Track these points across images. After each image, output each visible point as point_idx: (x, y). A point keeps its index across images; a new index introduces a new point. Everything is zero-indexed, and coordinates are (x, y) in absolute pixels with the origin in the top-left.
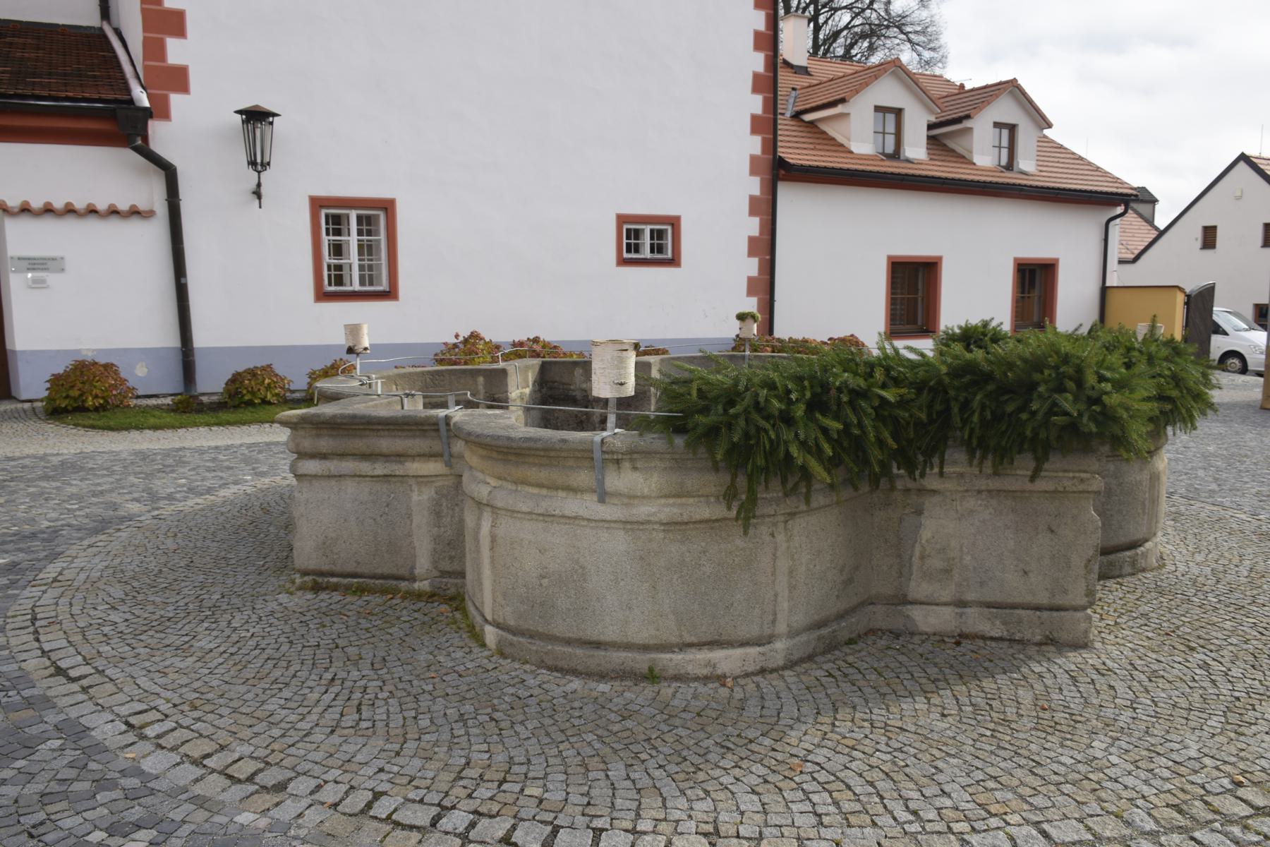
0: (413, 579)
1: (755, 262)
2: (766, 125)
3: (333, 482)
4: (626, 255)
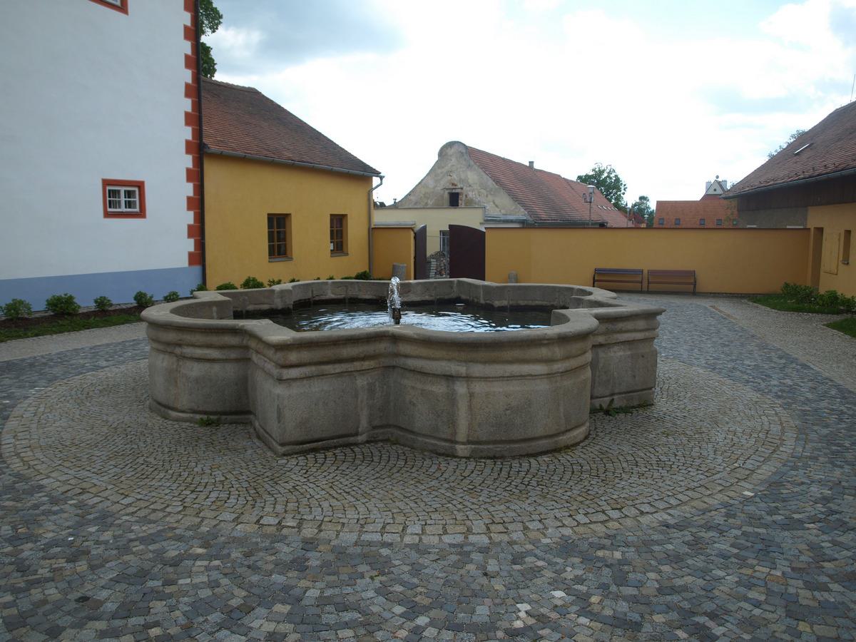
0: (357, 434)
1: (191, 214)
2: (195, 119)
3: (305, 382)
4: (137, 210)
